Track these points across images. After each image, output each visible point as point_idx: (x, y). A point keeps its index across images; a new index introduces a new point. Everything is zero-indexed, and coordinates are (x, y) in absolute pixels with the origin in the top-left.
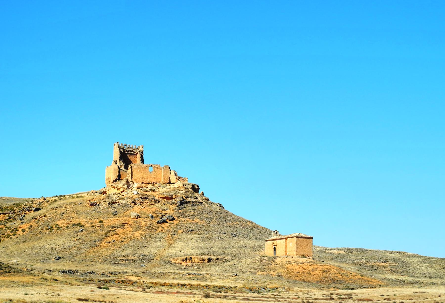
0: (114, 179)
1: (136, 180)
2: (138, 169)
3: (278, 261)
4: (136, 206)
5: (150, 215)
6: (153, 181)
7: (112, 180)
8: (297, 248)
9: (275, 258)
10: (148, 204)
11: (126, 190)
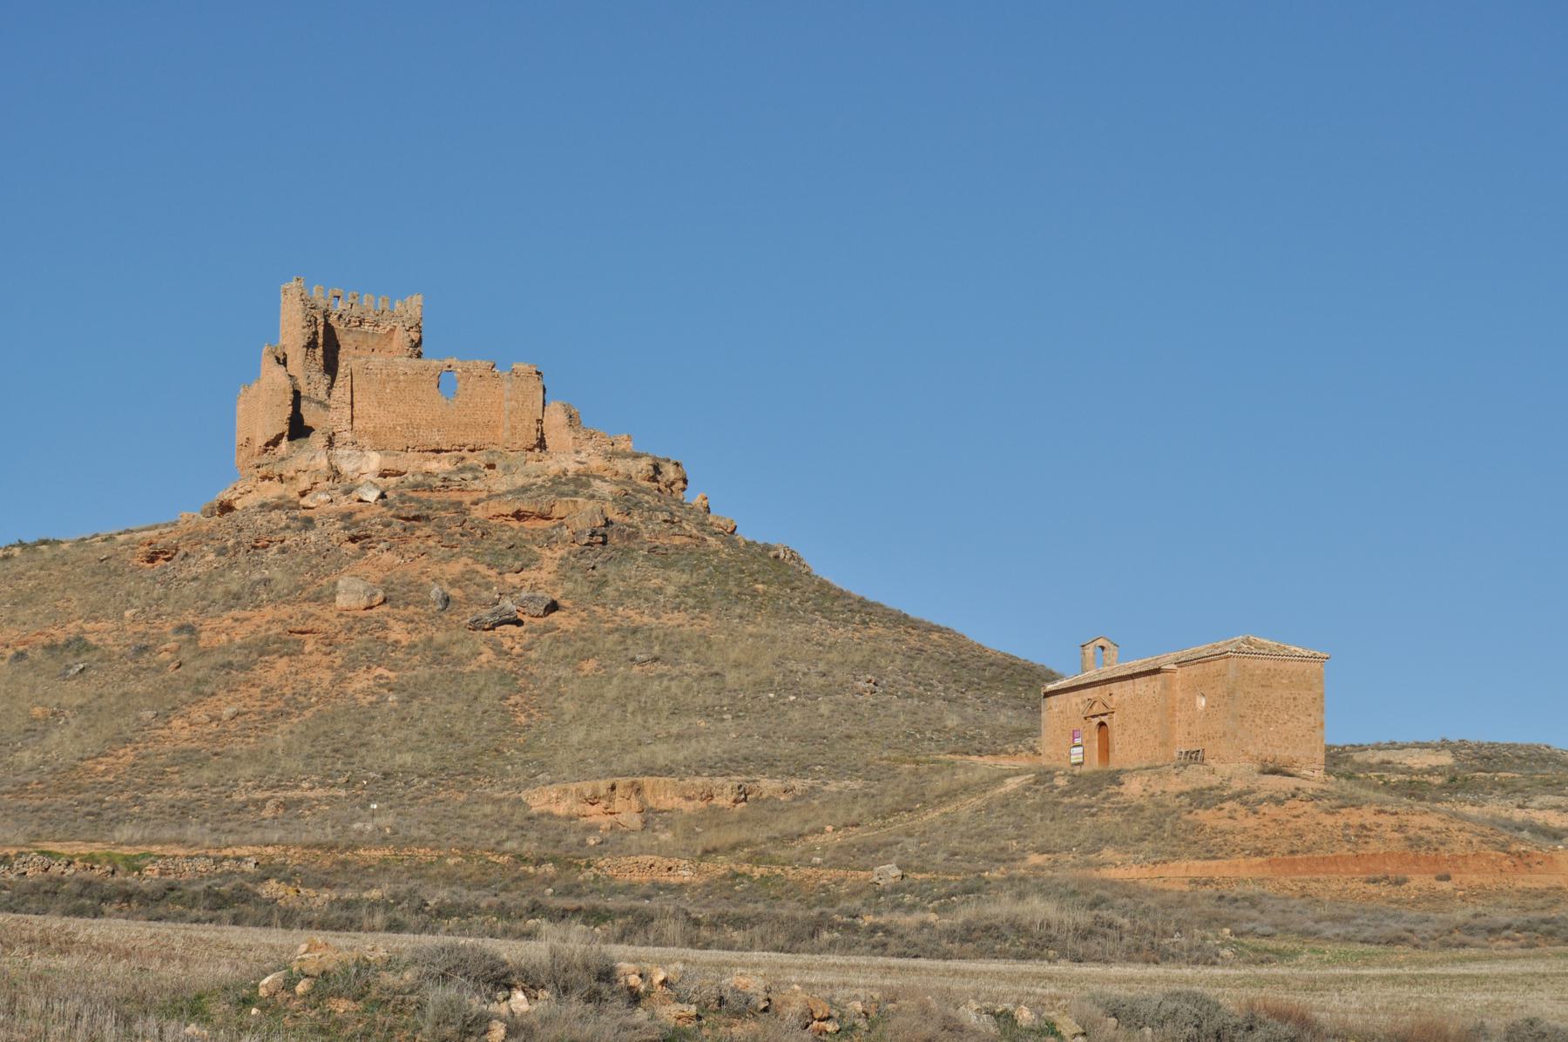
0: (271, 435)
1: (374, 434)
2: (384, 383)
3: (1133, 788)
4: (370, 553)
5: (435, 592)
6: (461, 441)
7: (260, 442)
8: (359, 929)
9: (1115, 778)
10: (431, 543)
11: (324, 484)
